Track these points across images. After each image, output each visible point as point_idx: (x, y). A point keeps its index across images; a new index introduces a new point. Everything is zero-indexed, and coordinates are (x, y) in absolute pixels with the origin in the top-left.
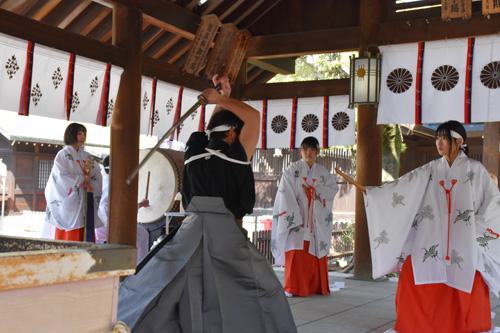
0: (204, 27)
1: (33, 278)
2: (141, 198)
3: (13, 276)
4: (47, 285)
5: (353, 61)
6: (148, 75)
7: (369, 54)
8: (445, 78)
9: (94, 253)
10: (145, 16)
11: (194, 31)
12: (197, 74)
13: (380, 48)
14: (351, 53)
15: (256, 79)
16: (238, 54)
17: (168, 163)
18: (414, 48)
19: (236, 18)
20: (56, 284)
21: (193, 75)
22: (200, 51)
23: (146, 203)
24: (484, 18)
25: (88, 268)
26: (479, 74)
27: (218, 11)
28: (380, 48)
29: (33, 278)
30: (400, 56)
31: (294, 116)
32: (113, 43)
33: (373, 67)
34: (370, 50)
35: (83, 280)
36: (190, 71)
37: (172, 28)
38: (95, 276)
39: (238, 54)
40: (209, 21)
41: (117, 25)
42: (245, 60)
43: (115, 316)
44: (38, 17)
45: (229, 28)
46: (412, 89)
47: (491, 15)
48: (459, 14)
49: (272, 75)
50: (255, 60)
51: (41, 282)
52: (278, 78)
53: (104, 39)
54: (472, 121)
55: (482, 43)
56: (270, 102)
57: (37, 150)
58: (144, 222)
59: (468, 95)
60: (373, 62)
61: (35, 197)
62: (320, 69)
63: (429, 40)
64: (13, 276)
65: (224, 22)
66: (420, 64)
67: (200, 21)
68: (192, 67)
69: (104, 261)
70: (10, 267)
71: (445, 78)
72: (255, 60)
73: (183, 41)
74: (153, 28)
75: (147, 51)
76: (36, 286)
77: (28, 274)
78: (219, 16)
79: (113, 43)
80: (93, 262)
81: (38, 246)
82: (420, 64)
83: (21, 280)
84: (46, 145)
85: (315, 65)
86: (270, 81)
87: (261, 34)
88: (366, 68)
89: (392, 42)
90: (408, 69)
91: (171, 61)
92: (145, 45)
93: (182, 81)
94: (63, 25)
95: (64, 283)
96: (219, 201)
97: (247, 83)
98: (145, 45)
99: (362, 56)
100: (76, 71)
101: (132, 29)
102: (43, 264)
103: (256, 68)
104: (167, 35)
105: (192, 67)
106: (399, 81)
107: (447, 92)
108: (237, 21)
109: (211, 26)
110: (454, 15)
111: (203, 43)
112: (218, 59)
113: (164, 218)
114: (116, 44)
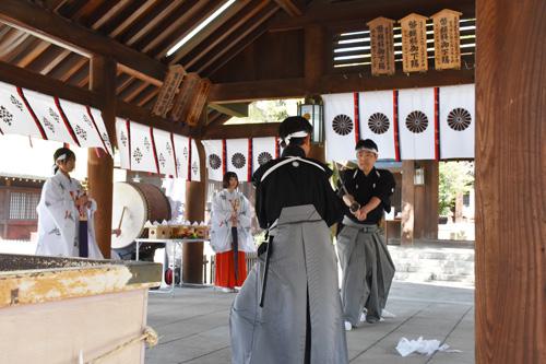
0: (171, 76)
1: (86, 289)
2: (115, 226)
3: (72, 286)
4: (97, 294)
5: (300, 106)
6: (121, 117)
7: (314, 101)
8: (417, 122)
9: (131, 267)
10: (119, 65)
11: (162, 78)
12: (164, 116)
13: (323, 96)
14: (298, 100)
15: (215, 120)
16: (200, 99)
17: (137, 193)
18: (350, 97)
19: (199, 67)
20: (103, 294)
21: (160, 117)
22: (167, 96)
23: (118, 232)
24: (405, 74)
25: (126, 281)
26: (446, 118)
27: (183, 62)
28: (323, 96)
29: (86, 289)
30: (339, 104)
31: (251, 153)
32: (90, 88)
33: (317, 112)
34: (315, 98)
35: (123, 291)
36: (158, 114)
37: (142, 76)
38: (132, 287)
39: (200, 99)
40: (176, 71)
41: (94, 73)
42: (206, 104)
43: (145, 322)
44: (22, 64)
45: (193, 77)
46: (353, 131)
47: (411, 73)
48: (451, 65)
49: (229, 117)
50: (215, 105)
51: (93, 292)
52: (235, 120)
53: (81, 84)
54: (442, 157)
55: (404, 95)
56: (228, 141)
57: (8, 184)
58: (120, 246)
59: (438, 136)
60: (317, 107)
61: (6, 227)
62: (269, 113)
63: (401, 88)
64: (72, 286)
65: (188, 71)
66: (357, 111)
67: (168, 70)
68: (160, 110)
69: (139, 275)
70: (70, 279)
71: (417, 122)
72: (215, 105)
73: (152, 87)
74: (125, 75)
75: (120, 94)
76: (88, 295)
77: (84, 285)
78: (184, 65)
79: (90, 88)
80: (131, 275)
81: (75, 263)
82: (357, 111)
83: (78, 290)
84: (17, 179)
85: (265, 110)
86: (226, 124)
87: (221, 82)
88: (311, 113)
89: (332, 92)
90: (466, 109)
91: (140, 105)
92: (119, 89)
93: (153, 122)
94: (44, 72)
95: (109, 293)
96: (310, 208)
97: (208, 123)
98: (119, 89)
99: (307, 103)
100: (441, 100)
101: (108, 75)
102: (93, 277)
103: (215, 111)
104: (137, 81)
105: (160, 110)
106: (343, 125)
107: (453, 130)
108: (201, 70)
109: (177, 74)
110: (382, 71)
111: (170, 89)
112: (183, 103)
113: (134, 243)
114: (93, 88)
